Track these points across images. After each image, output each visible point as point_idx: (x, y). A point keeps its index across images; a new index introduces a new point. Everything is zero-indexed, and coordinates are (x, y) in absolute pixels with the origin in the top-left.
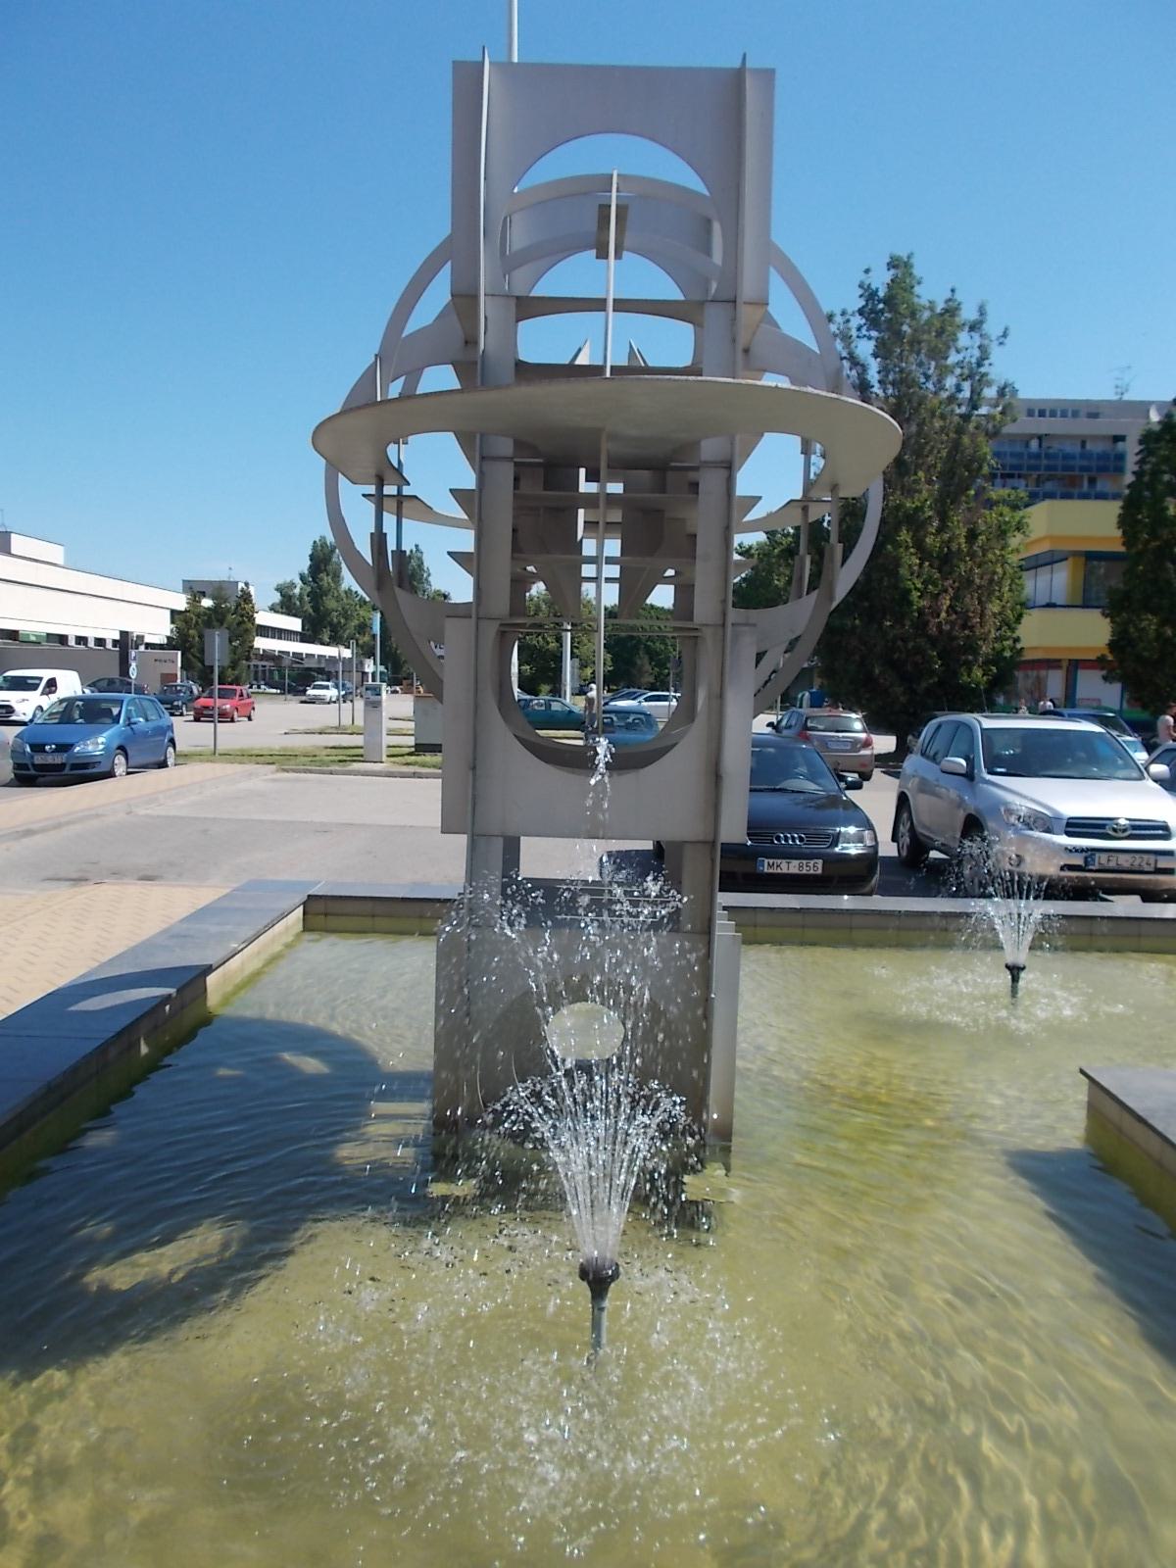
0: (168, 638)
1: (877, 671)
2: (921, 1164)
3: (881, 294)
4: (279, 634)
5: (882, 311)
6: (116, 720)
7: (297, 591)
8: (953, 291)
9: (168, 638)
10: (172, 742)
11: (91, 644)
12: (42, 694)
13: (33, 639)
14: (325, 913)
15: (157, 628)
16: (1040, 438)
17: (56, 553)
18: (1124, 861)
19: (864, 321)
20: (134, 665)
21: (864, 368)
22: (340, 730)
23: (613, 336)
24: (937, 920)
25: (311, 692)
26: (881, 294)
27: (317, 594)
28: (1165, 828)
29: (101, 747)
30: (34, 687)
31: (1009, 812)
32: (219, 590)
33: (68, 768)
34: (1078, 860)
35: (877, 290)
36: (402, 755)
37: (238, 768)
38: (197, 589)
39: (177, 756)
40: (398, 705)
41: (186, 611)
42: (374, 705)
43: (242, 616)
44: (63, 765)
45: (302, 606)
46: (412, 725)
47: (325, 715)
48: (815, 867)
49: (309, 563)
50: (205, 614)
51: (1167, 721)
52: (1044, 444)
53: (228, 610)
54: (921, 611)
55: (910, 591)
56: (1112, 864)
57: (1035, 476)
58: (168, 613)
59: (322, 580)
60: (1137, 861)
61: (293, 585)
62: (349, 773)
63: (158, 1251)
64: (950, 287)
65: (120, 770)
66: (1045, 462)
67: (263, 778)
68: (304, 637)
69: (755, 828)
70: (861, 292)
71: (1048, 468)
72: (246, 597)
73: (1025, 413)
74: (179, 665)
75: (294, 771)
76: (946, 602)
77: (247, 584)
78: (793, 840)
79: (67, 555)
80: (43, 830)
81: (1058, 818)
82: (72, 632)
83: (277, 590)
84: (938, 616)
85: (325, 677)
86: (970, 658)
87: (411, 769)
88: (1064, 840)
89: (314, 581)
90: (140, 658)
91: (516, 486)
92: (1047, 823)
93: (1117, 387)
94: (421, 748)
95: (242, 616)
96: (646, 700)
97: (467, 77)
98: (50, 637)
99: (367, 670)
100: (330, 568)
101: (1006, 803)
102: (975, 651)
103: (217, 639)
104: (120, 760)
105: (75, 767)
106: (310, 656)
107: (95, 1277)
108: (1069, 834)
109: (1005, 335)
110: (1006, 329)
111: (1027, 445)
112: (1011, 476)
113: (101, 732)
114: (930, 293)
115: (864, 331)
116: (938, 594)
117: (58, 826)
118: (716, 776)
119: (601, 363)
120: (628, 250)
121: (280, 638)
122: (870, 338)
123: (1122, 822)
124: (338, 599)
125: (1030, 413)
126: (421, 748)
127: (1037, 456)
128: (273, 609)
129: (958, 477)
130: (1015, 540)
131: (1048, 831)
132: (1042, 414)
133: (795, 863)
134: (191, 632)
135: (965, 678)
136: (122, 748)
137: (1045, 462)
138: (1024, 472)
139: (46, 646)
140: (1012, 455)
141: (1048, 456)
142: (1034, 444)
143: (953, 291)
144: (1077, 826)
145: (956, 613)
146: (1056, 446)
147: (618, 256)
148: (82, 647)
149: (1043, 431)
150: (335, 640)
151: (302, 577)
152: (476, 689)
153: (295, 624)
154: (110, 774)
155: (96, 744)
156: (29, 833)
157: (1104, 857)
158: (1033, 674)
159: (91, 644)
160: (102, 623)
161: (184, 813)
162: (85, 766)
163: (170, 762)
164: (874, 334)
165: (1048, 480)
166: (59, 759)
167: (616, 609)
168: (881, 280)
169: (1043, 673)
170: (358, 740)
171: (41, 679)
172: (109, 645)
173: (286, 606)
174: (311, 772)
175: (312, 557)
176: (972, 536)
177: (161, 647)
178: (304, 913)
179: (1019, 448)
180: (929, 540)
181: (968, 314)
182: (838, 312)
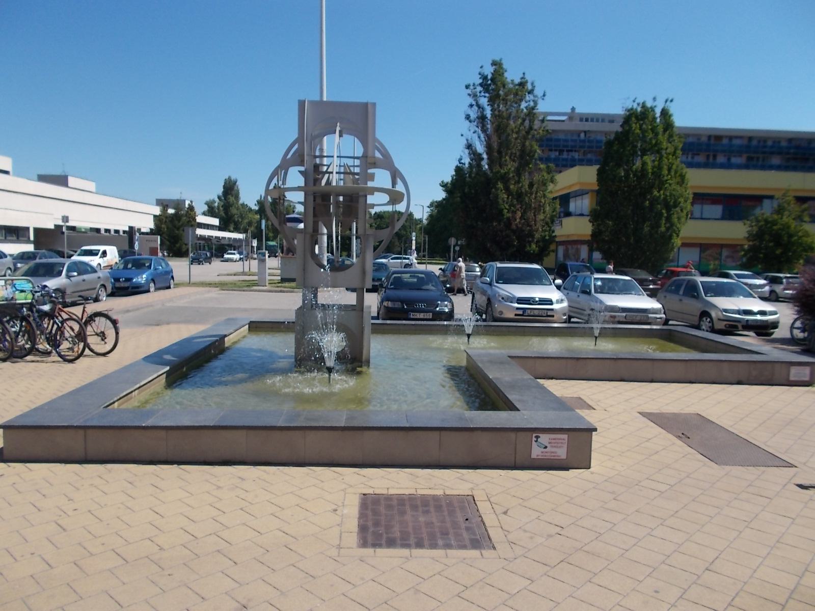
0: (151, 229)
1: (489, 245)
3: (489, 77)
4: (208, 227)
5: (490, 85)
6: (149, 267)
7: (216, 204)
8: (524, 74)
9: (151, 229)
10: (173, 277)
11: (112, 232)
12: (100, 257)
13: (83, 230)
14: (256, 327)
15: (147, 224)
16: (585, 132)
17: (91, 186)
18: (536, 312)
19: (482, 89)
20: (137, 243)
21: (483, 109)
22: (244, 273)
25: (226, 256)
26: (489, 77)
27: (227, 206)
28: (551, 301)
29: (144, 279)
30: (97, 254)
31: (499, 295)
32: (178, 204)
33: (130, 288)
34: (520, 312)
35: (487, 75)
36: (275, 283)
37: (207, 289)
38: (165, 204)
39: (174, 284)
40: (273, 263)
41: (160, 215)
42: (262, 261)
43: (189, 218)
44: (128, 288)
45: (219, 212)
46: (279, 271)
47: (238, 267)
48: (430, 316)
49: (222, 190)
50: (170, 217)
51: (610, 268)
52: (587, 135)
53: (182, 215)
54: (508, 219)
55: (503, 209)
56: (532, 314)
57: (582, 151)
58: (152, 217)
59: (229, 198)
60: (540, 313)
61: (214, 201)
62: (256, 291)
64: (522, 72)
65: (152, 289)
66: (587, 144)
67: (215, 293)
68: (220, 228)
70: (480, 76)
71: (589, 147)
72: (191, 208)
73: (579, 120)
74: (159, 243)
75: (227, 290)
76: (519, 214)
77: (191, 202)
78: (422, 306)
79: (97, 187)
80: (133, 310)
81: (514, 297)
82: (102, 227)
83: (206, 204)
84: (516, 220)
85: (232, 248)
86: (530, 239)
87: (279, 289)
88: (516, 305)
89: (225, 199)
90: (139, 240)
91: (314, 201)
92: (511, 299)
93: (623, 107)
94: (283, 280)
95: (189, 218)
96: (392, 259)
97: (302, 104)
98: (92, 229)
99: (253, 245)
100: (233, 192)
101: (499, 293)
102: (533, 236)
103: (190, 232)
104: (152, 285)
105: (133, 288)
108: (518, 303)
109: (544, 95)
110: (545, 92)
111: (579, 136)
112: (571, 151)
113: (143, 273)
114: (512, 76)
115: (482, 94)
116: (34, 295)
117: (138, 309)
118: (364, 272)
121: (208, 229)
122: (485, 97)
123: (537, 299)
124: (238, 209)
125: (581, 120)
126: (283, 280)
127: (584, 141)
128: (204, 214)
129: (525, 159)
130: (551, 187)
131: (511, 302)
132: (587, 120)
133: (422, 314)
134: (163, 226)
135: (528, 248)
136: (153, 280)
137: (587, 144)
138: (577, 149)
139: (90, 234)
140: (572, 140)
141: (589, 141)
142: (582, 135)
143: (524, 74)
144: (520, 300)
145: (524, 219)
146: (593, 137)
147: (341, 136)
148: (108, 234)
149: (586, 129)
150: (237, 230)
151: (219, 197)
153: (215, 222)
154: (148, 291)
155: (142, 278)
156: (128, 311)
157: (529, 311)
158: (575, 247)
159: (112, 232)
160: (120, 222)
161: (186, 305)
162: (138, 287)
163: (172, 286)
164: (487, 95)
165: (589, 153)
166: (127, 284)
168: (489, 71)
169: (579, 246)
170: (256, 278)
171: (99, 250)
172: (121, 233)
173: (211, 212)
174: (235, 290)
175: (224, 187)
176: (531, 185)
177: (147, 234)
178: (249, 327)
179: (575, 137)
180: (512, 187)
181: (529, 87)
182: (472, 84)
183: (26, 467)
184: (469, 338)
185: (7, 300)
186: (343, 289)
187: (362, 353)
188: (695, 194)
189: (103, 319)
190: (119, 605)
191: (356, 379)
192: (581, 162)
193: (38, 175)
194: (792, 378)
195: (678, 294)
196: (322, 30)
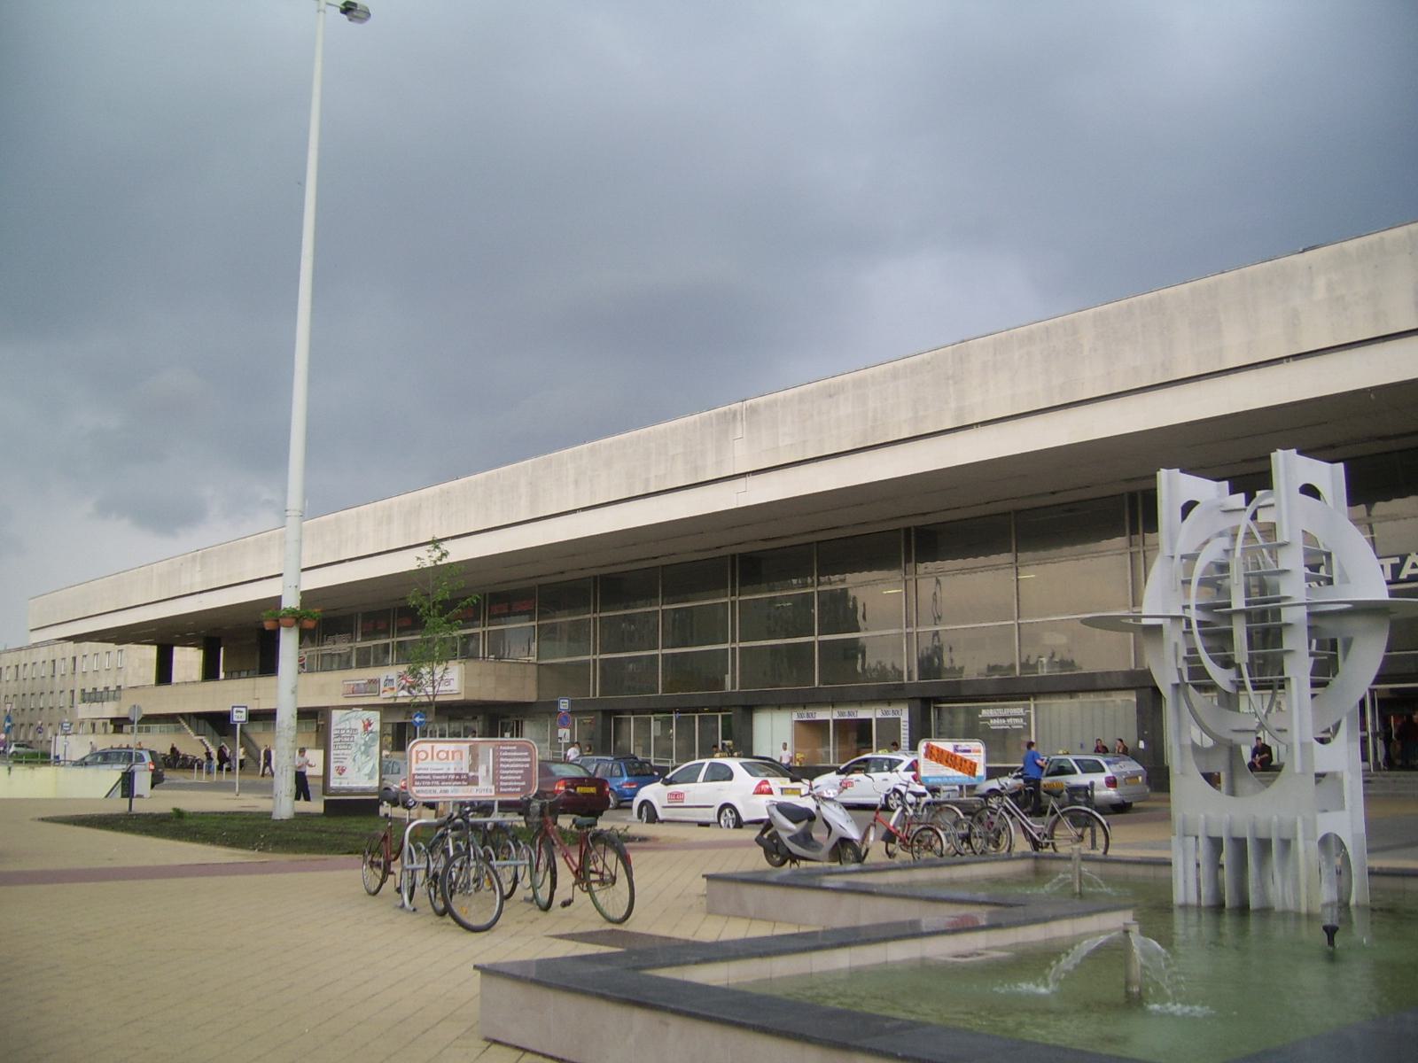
2: (501, 747)
23: (902, 609)
24: (218, 815)
63: (1090, 1049)
69: (1019, 628)
106: (643, 606)
107: (1206, 1010)
119: (1133, 536)
120: (1137, 602)
152: (822, 530)
167: (1220, 663)
183: (1202, 736)
184: (969, 842)
185: (753, 410)
186: (516, 814)
187: (260, 658)
188: (297, 798)
189: (474, 922)
190: (1013, 498)
191: (1148, 1003)
192: (277, 820)
193: (1271, 488)
194: (1305, 607)
195: (351, 668)
196: (1036, 725)
